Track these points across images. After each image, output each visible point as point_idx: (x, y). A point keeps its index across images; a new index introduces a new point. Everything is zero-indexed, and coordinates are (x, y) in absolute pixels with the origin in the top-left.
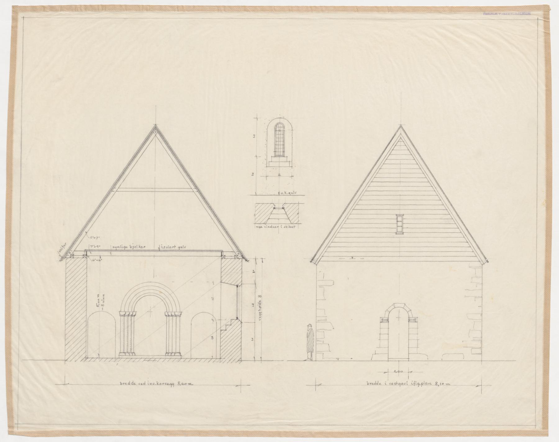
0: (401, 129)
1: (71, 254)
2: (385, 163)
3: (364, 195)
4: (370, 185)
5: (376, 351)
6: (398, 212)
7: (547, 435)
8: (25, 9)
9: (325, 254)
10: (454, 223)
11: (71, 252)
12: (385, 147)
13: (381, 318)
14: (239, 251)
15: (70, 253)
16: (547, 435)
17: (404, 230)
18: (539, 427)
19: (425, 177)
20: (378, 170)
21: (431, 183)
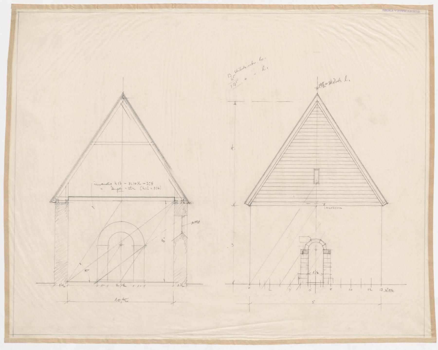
0: (317, 97)
1: (56, 199)
2: (259, 193)
3: (261, 190)
4: (259, 193)
5: (299, 273)
6: (315, 167)
7: (435, 342)
8: (24, 6)
9: (302, 127)
10: (343, 146)
11: (57, 198)
12: (83, 198)
13: (302, 251)
14: (185, 197)
15: (56, 198)
16: (435, 342)
17: (320, 181)
18: (428, 336)
19: (343, 146)
20: (299, 130)
21: (344, 143)
